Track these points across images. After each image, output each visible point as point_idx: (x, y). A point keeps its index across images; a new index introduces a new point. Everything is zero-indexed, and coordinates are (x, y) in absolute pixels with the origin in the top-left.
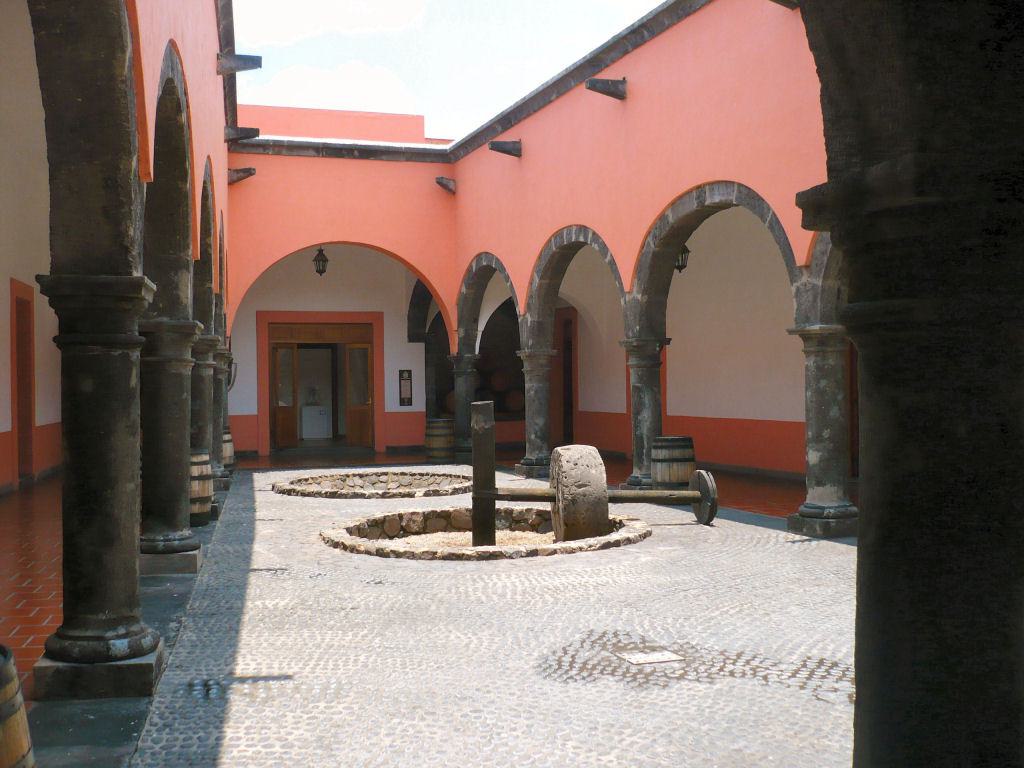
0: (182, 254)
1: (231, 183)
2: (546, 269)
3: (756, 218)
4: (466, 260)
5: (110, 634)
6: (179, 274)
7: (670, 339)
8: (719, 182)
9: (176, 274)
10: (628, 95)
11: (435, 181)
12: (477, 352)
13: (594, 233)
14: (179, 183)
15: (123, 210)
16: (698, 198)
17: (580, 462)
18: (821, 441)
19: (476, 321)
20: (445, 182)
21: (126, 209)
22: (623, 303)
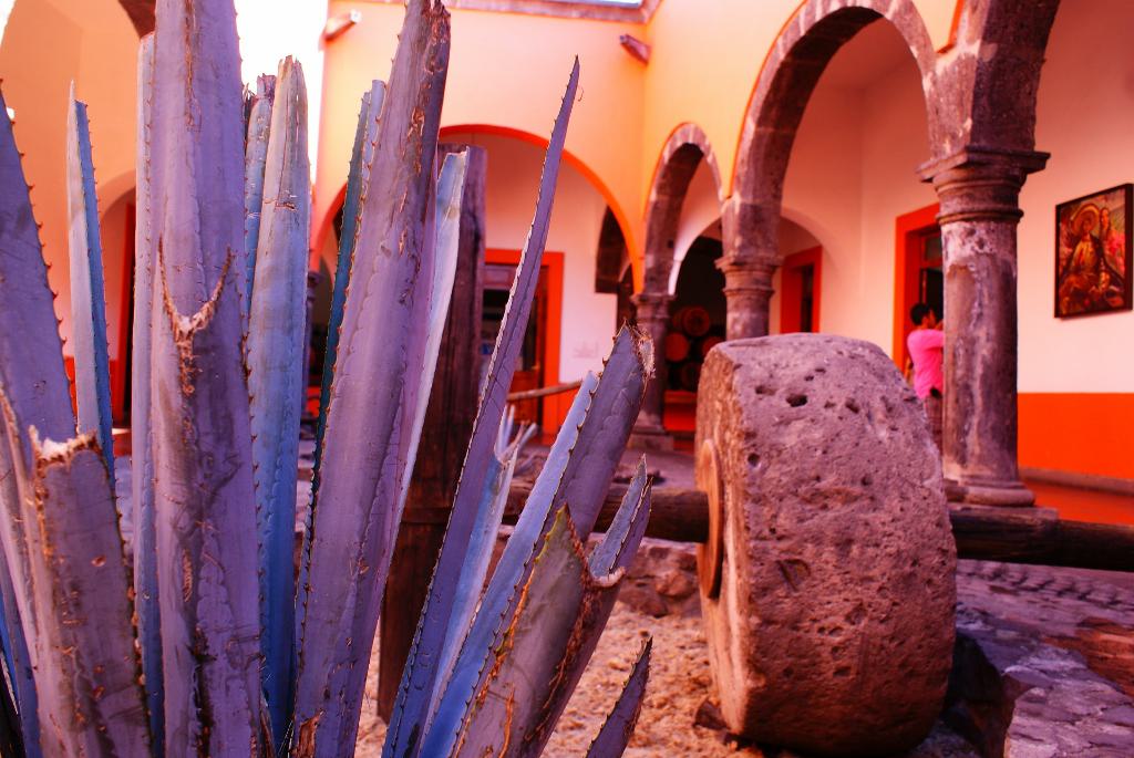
1: (579, 387)
2: (768, 104)
4: (657, 150)
7: (1044, 157)
11: (619, 42)
12: (672, 289)
17: (818, 392)
19: (671, 245)
20: (633, 43)
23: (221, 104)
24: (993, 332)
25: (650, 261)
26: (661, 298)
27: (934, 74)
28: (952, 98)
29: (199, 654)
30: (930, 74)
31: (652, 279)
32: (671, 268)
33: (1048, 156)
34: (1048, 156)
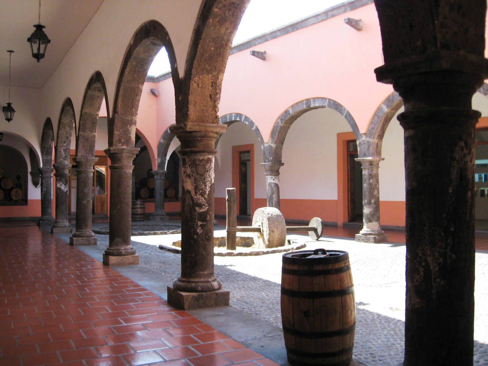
0: (134, 118)
3: (338, 114)
5: (210, 280)
6: (132, 127)
8: (318, 98)
9: (130, 127)
10: (267, 59)
11: (150, 91)
12: (166, 170)
13: (246, 117)
14: (140, 85)
15: (217, 96)
16: (307, 104)
18: (371, 204)
19: (166, 155)
20: (154, 91)
21: (218, 96)
22: (262, 147)
23: (391, 267)
24: (276, 196)
25: (159, 160)
26: (163, 172)
27: (264, 146)
28: (268, 152)
29: (198, 282)
30: (263, 146)
31: (160, 166)
32: (165, 163)
33: (284, 163)
34: (284, 163)
